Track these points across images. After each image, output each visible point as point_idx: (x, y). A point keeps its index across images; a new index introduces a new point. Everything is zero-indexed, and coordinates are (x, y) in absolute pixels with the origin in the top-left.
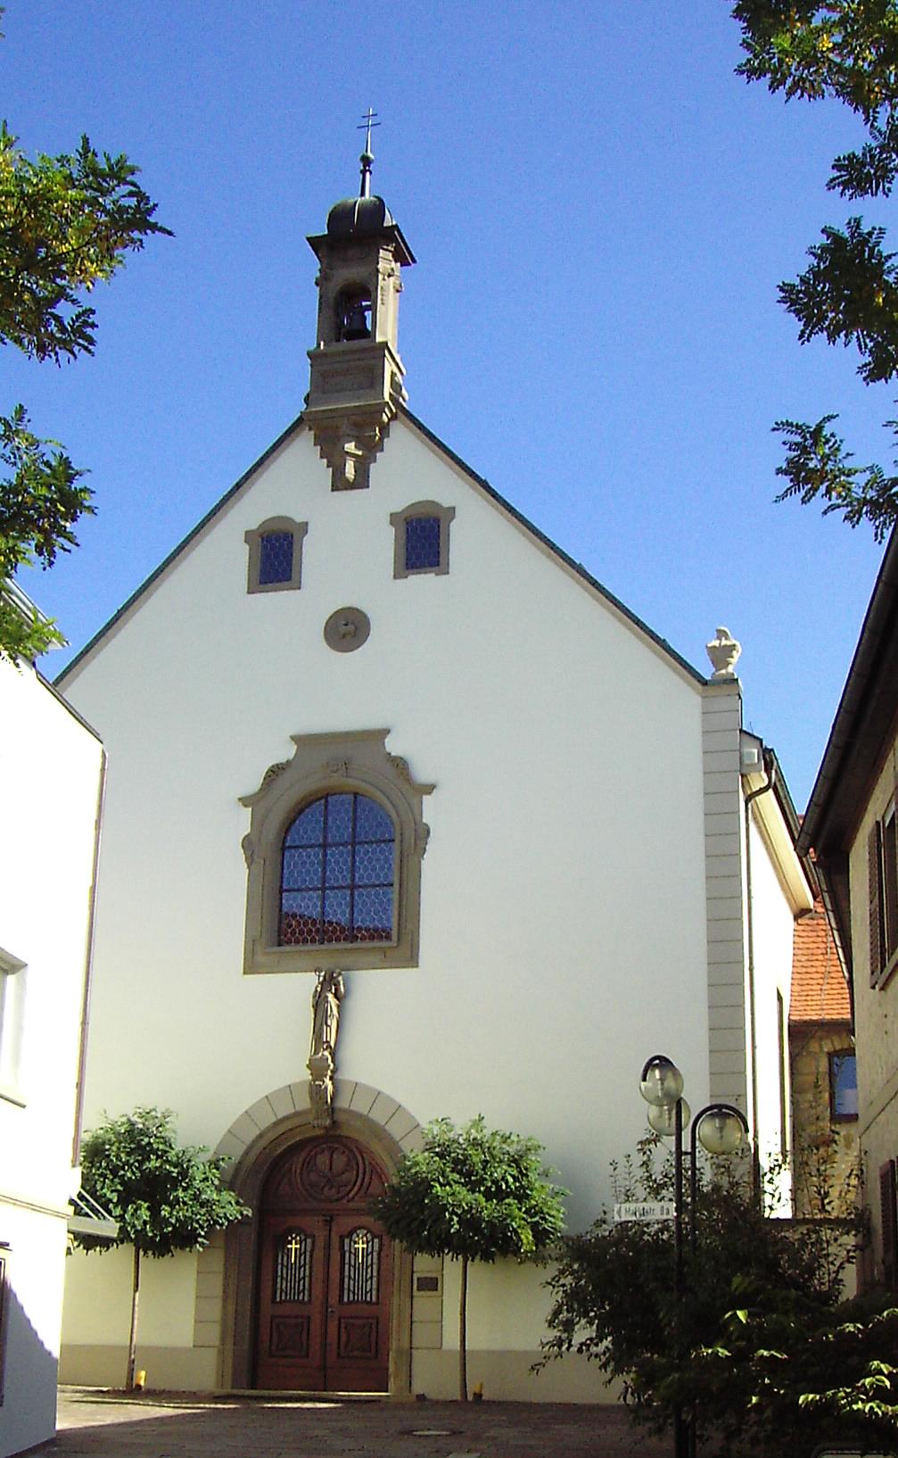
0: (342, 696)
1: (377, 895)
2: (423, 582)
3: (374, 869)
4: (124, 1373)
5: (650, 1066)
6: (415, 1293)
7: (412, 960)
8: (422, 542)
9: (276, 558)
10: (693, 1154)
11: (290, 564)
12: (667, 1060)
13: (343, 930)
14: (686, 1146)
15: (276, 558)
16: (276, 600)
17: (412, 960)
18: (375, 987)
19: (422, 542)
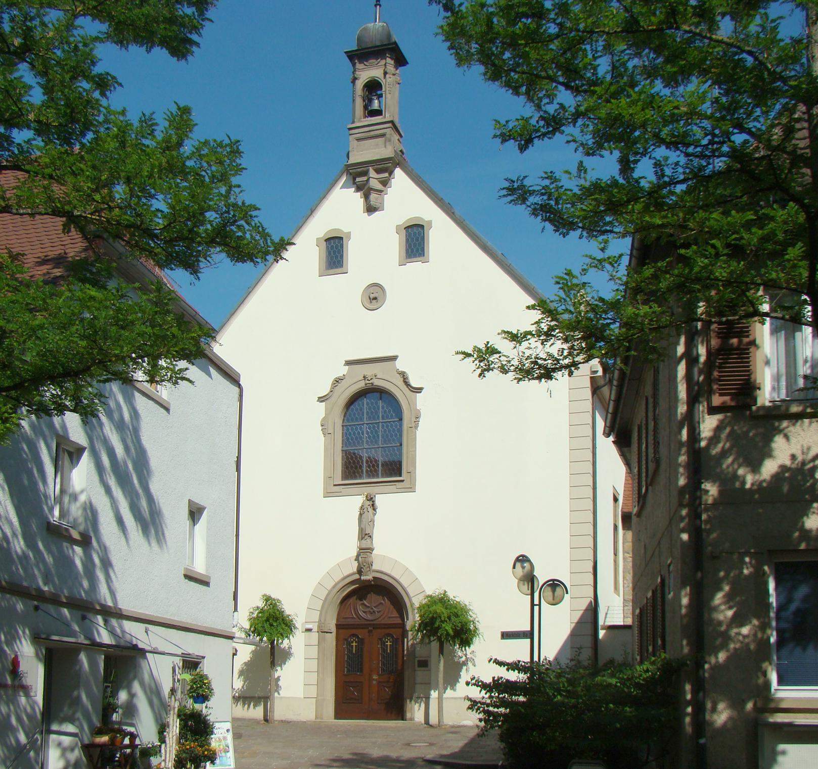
0: (370, 336)
1: (392, 426)
2: (415, 266)
3: (389, 431)
4: (352, 547)
5: (517, 560)
6: (417, 668)
7: (411, 489)
8: (415, 241)
9: (334, 252)
10: (540, 605)
11: (342, 256)
12: (526, 557)
13: (60, 212)
14: (536, 602)
15: (334, 252)
16: (335, 280)
17: (411, 489)
18: (389, 502)
19: (415, 241)
